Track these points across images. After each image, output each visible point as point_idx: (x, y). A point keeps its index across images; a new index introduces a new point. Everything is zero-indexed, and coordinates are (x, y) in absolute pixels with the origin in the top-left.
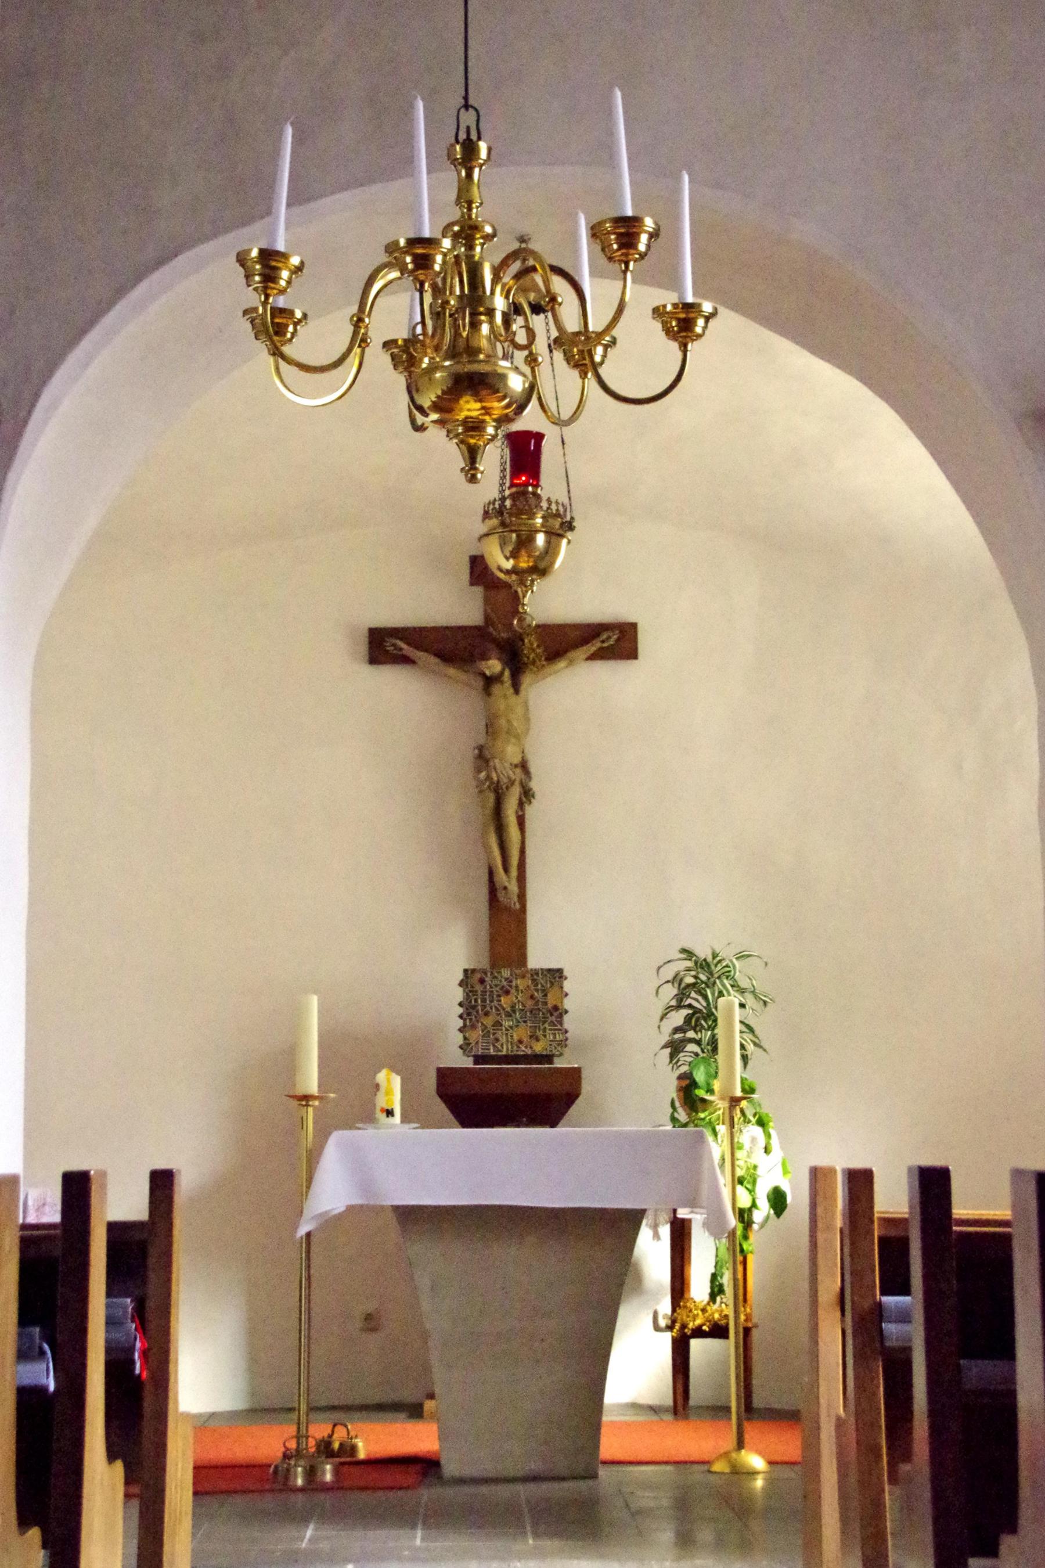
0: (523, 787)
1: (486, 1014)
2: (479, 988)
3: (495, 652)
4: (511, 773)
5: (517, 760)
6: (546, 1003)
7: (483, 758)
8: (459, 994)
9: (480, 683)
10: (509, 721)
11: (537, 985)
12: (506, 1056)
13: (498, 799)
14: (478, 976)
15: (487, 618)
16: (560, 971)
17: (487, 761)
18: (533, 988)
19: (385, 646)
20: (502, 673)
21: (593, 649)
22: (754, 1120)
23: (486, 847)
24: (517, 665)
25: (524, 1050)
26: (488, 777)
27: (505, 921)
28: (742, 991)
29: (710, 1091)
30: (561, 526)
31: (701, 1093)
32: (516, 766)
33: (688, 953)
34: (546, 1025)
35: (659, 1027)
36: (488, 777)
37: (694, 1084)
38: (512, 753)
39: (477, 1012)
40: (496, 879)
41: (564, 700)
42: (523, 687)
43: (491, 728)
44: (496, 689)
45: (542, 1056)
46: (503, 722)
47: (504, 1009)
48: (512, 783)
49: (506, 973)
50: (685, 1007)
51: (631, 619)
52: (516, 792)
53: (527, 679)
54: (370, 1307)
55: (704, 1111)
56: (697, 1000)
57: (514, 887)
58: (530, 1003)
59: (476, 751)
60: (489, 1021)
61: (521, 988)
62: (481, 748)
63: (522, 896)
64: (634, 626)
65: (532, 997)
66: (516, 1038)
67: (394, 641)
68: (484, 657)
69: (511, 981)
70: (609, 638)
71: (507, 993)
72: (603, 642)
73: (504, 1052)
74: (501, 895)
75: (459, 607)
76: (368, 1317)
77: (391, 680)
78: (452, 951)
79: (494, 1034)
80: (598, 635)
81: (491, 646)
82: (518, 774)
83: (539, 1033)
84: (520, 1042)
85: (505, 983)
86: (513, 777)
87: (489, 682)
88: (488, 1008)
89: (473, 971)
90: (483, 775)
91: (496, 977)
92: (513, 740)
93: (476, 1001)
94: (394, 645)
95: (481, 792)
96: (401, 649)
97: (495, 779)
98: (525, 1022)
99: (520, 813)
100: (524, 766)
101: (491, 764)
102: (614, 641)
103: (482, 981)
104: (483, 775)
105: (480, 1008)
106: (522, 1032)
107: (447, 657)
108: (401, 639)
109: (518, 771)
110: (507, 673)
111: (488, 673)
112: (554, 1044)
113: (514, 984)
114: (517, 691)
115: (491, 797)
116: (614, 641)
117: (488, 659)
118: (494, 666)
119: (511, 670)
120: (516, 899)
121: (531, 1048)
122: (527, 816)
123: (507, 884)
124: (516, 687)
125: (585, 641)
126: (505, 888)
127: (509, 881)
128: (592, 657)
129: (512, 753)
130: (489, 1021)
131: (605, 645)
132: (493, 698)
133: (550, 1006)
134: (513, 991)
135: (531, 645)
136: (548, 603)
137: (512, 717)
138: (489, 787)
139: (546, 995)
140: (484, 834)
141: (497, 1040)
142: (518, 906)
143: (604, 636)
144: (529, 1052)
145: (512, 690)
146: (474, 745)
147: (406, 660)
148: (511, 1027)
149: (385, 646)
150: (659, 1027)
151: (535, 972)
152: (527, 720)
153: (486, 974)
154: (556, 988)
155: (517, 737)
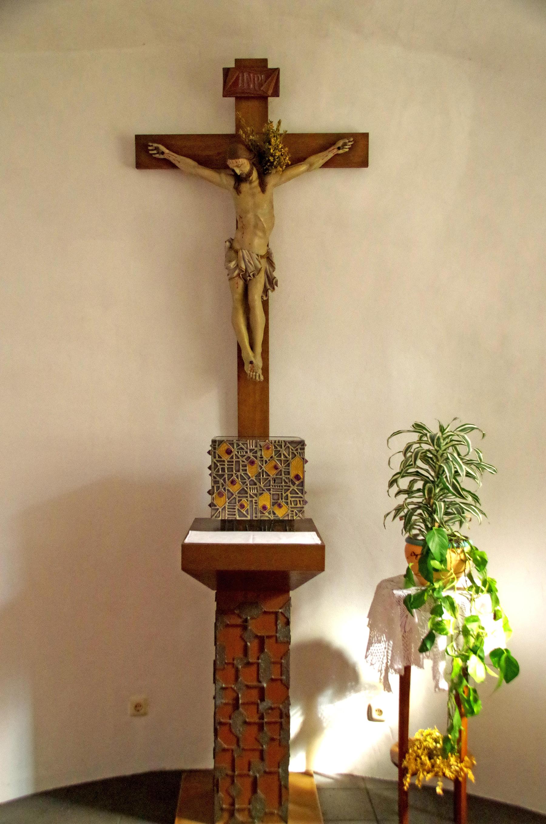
0: (268, 277)
1: (233, 482)
2: (226, 458)
3: (242, 150)
4: (257, 262)
5: (263, 252)
6: (289, 473)
7: (233, 249)
8: (208, 460)
9: (230, 182)
10: (257, 217)
11: (280, 456)
12: (251, 521)
13: (245, 288)
14: (224, 447)
15: (238, 126)
16: (301, 444)
17: (237, 252)
18: (276, 458)
19: (150, 153)
20: (250, 174)
21: (331, 155)
22: (485, 589)
23: (238, 332)
24: (264, 164)
25: (267, 516)
26: (238, 266)
27: (251, 394)
28: (469, 463)
29: (443, 561)
30: (306, 493)
31: (435, 564)
32: (262, 257)
33: (419, 427)
34: (288, 493)
35: (388, 491)
36: (238, 266)
37: (426, 554)
38: (258, 245)
39: (224, 480)
40: (244, 355)
41: (305, 206)
42: (269, 187)
43: (240, 224)
44: (245, 187)
45: (283, 521)
46: (250, 216)
47: (249, 478)
48: (259, 271)
49: (251, 444)
50: (411, 474)
51: (362, 130)
52: (261, 279)
53: (272, 180)
54: (137, 698)
55: (438, 580)
56: (427, 471)
57: (259, 362)
58: (273, 473)
59: (228, 243)
60: (235, 489)
61: (265, 458)
62: (231, 241)
63: (266, 370)
64: (364, 163)
65: (276, 468)
66: (260, 504)
67: (156, 145)
68: (235, 156)
69: (256, 452)
70: (345, 144)
71: (252, 463)
72: (339, 148)
73: (249, 518)
74: (247, 368)
75: (209, 116)
76: (137, 707)
77: (156, 186)
78: (203, 419)
79: (239, 501)
80: (334, 144)
81: (241, 146)
82: (263, 264)
83: (282, 502)
84: (264, 508)
85: (250, 454)
86: (259, 266)
87: (239, 180)
88: (234, 477)
89: (221, 442)
90: (232, 265)
91: (242, 449)
92: (260, 234)
93: (223, 470)
94: (157, 149)
95: (231, 279)
96: (163, 153)
97: (243, 267)
98: (269, 490)
99: (265, 298)
100: (268, 257)
101: (240, 254)
102: (349, 151)
103: (229, 452)
104: (232, 265)
105: (226, 476)
106: (266, 500)
107: (204, 162)
108: (163, 145)
109: (264, 262)
110: (255, 175)
111: (238, 171)
112: (295, 510)
113: (259, 454)
114: (263, 190)
115: (241, 283)
116: (349, 151)
117: (238, 157)
118: (242, 165)
119: (258, 170)
120: (260, 372)
121: (274, 514)
122: (270, 301)
123: (253, 359)
124: (263, 186)
125: (324, 148)
126: (251, 363)
127: (255, 357)
128: (326, 165)
129: (258, 245)
130: (235, 489)
131: (341, 152)
132: (242, 195)
133: (292, 476)
134: (258, 462)
135: (278, 150)
136: (295, 113)
137: (260, 212)
138: (239, 275)
139: (288, 465)
140: (235, 309)
141: (242, 506)
142: (262, 378)
143: (340, 143)
144: (272, 517)
145: (259, 189)
146: (227, 238)
147: (170, 165)
148: (256, 495)
149: (150, 153)
150: (388, 491)
151: (279, 444)
152: (272, 217)
153: (232, 444)
154: (297, 459)
155: (264, 231)
